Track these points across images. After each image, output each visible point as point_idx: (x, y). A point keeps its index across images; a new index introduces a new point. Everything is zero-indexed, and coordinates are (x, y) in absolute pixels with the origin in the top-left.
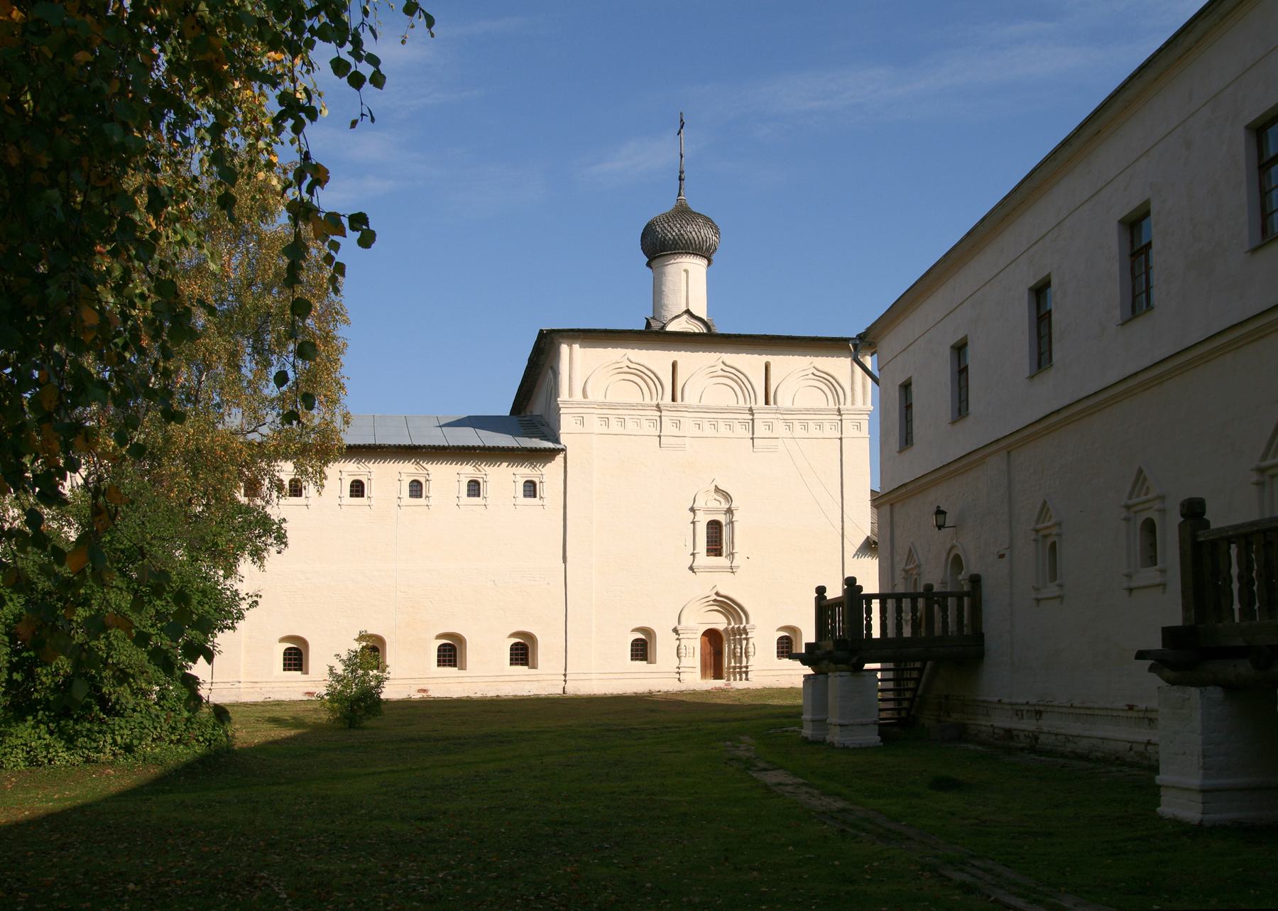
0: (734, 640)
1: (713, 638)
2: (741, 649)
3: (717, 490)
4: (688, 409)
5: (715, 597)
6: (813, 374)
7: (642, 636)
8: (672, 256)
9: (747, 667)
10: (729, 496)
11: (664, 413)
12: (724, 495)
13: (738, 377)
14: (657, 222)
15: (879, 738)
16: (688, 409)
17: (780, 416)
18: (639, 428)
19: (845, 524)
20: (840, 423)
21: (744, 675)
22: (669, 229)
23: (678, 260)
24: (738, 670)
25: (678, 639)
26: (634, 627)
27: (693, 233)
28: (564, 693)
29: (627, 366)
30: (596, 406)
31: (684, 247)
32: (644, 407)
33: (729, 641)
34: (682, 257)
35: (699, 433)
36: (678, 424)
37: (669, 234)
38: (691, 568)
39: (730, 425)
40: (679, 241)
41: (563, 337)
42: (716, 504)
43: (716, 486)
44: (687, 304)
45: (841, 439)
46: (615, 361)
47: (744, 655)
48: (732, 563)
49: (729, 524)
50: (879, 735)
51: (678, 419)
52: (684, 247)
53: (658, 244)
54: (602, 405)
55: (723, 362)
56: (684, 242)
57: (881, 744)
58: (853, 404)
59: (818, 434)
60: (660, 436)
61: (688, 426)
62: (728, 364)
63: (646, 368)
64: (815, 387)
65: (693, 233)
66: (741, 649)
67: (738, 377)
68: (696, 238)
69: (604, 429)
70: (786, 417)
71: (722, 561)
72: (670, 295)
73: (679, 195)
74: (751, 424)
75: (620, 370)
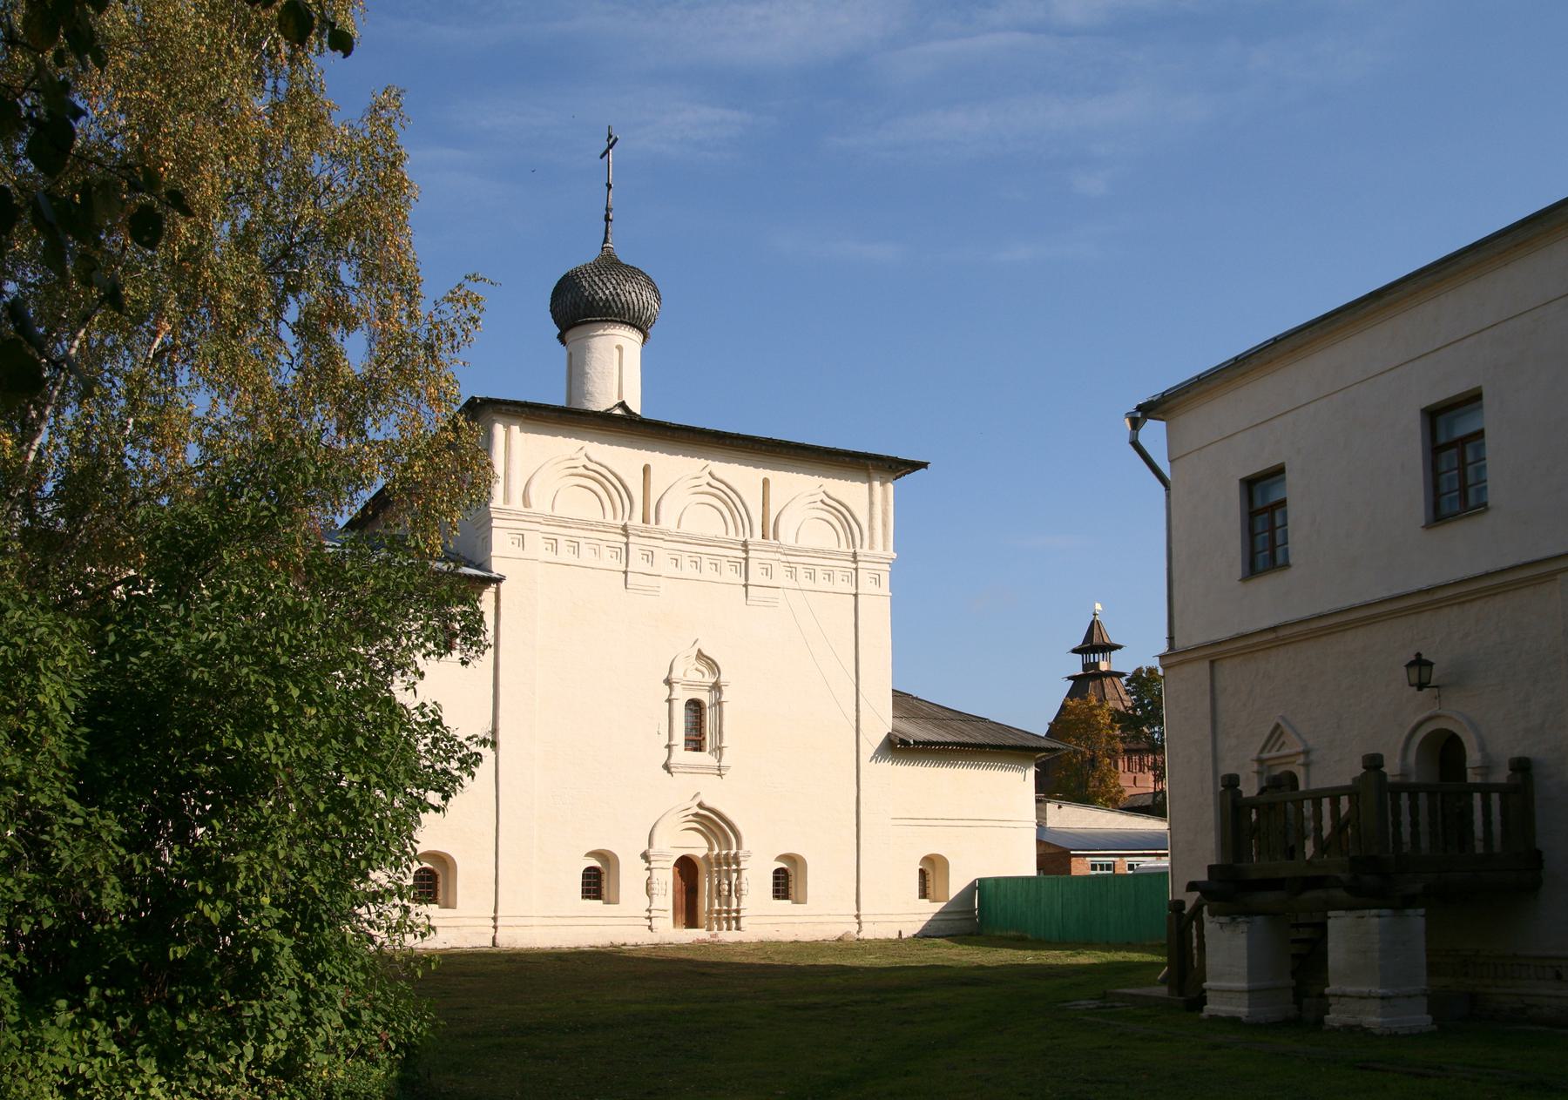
0: (719, 872)
1: (687, 868)
2: (730, 884)
3: (700, 655)
4: (665, 536)
5: (697, 810)
6: (822, 501)
7: (597, 864)
8: (601, 324)
9: (738, 911)
10: (717, 665)
11: (632, 539)
12: (708, 663)
13: (728, 497)
14: (582, 273)
15: (1429, 1018)
16: (665, 536)
17: (784, 558)
18: (597, 558)
19: (861, 713)
20: (854, 572)
21: (734, 922)
22: (600, 284)
23: (609, 331)
24: (725, 915)
25: (648, 869)
26: (590, 850)
27: (633, 294)
28: (494, 944)
29: (584, 466)
30: (541, 520)
31: (619, 312)
32: (604, 528)
33: (710, 874)
34: (609, 327)
35: (676, 572)
36: (650, 557)
37: (600, 292)
38: (667, 767)
39: (716, 565)
40: (613, 304)
41: (499, 412)
42: (698, 677)
43: (699, 651)
44: (620, 395)
45: (856, 595)
46: (568, 457)
47: (733, 894)
48: (719, 761)
49: (715, 705)
50: (1428, 1013)
51: (651, 549)
52: (619, 312)
53: (582, 305)
54: (551, 520)
55: (710, 473)
56: (620, 306)
57: (1435, 1027)
58: (871, 547)
59: (827, 586)
60: (625, 573)
61: (663, 563)
62: (717, 476)
63: (610, 471)
64: (824, 520)
65: (633, 294)
66: (730, 884)
67: (728, 497)
68: (636, 303)
69: (551, 556)
70: (791, 559)
71: (704, 758)
72: (595, 379)
73: (606, 241)
74: (743, 565)
75: (574, 471)
